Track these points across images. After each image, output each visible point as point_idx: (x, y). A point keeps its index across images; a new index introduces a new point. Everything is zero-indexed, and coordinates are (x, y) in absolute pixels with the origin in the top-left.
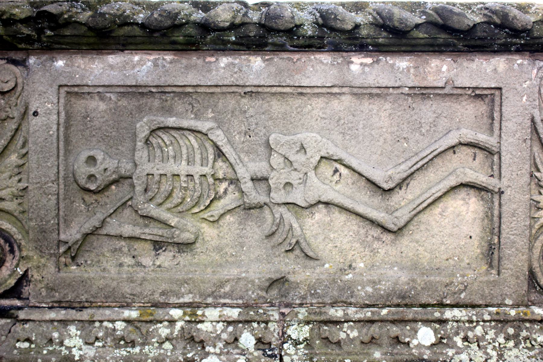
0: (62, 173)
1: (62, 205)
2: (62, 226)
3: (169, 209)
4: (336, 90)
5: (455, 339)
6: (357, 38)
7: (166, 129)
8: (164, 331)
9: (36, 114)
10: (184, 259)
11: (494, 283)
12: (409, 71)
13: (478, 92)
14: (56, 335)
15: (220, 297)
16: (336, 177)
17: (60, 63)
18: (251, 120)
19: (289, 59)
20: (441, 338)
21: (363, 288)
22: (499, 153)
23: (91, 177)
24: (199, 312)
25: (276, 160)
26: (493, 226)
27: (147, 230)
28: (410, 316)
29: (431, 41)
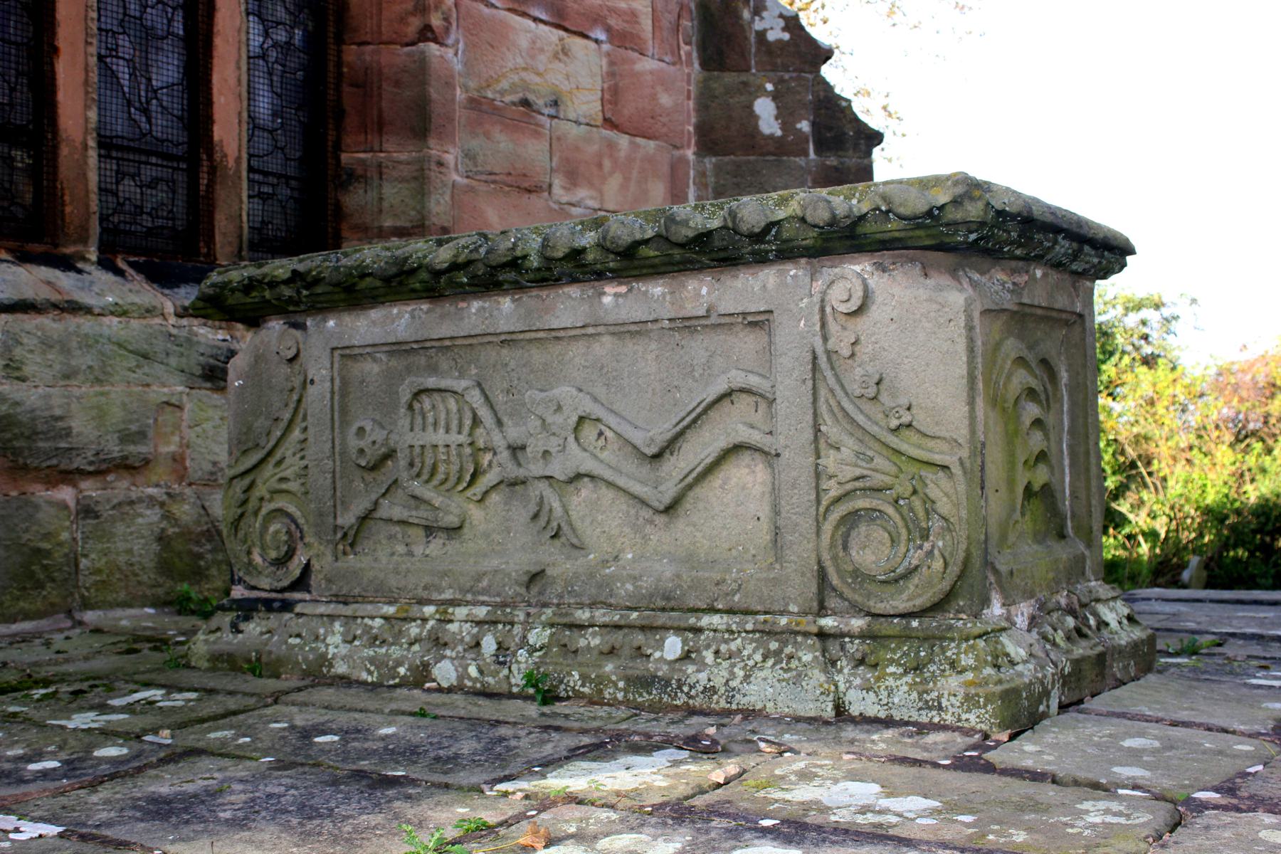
0: (337, 449)
1: (339, 485)
2: (339, 507)
4: (590, 330)
5: (704, 653)
6: (584, 266)
7: (427, 391)
8: (414, 630)
10: (453, 547)
11: (776, 582)
12: (664, 298)
13: (750, 319)
14: (322, 631)
15: (479, 593)
16: (601, 442)
17: (331, 323)
18: (513, 374)
19: (538, 296)
20: (689, 651)
21: (623, 584)
24: (450, 610)
27: (414, 513)
28: (659, 623)
29: (666, 259)
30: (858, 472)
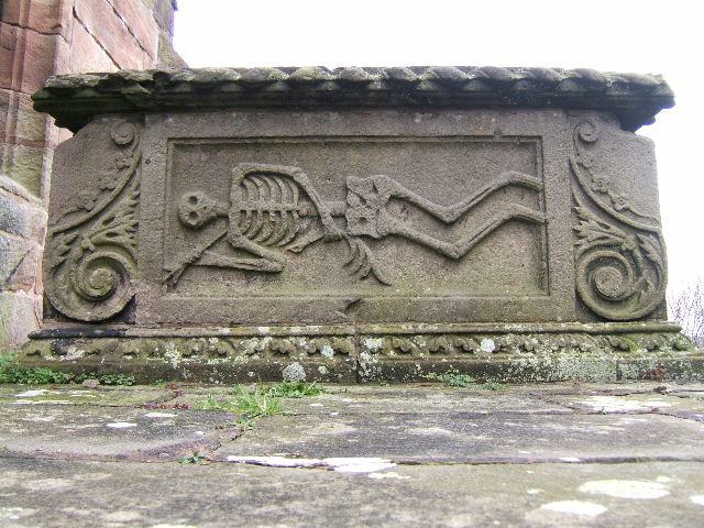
3: (259, 243)
9: (148, 162)
11: (548, 304)
19: (450, 119)
20: (502, 347)
22: (543, 190)
23: (193, 215)
25: (353, 199)
26: (542, 255)
30: (600, 234)
